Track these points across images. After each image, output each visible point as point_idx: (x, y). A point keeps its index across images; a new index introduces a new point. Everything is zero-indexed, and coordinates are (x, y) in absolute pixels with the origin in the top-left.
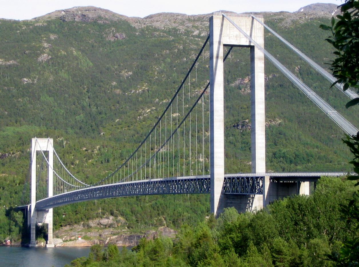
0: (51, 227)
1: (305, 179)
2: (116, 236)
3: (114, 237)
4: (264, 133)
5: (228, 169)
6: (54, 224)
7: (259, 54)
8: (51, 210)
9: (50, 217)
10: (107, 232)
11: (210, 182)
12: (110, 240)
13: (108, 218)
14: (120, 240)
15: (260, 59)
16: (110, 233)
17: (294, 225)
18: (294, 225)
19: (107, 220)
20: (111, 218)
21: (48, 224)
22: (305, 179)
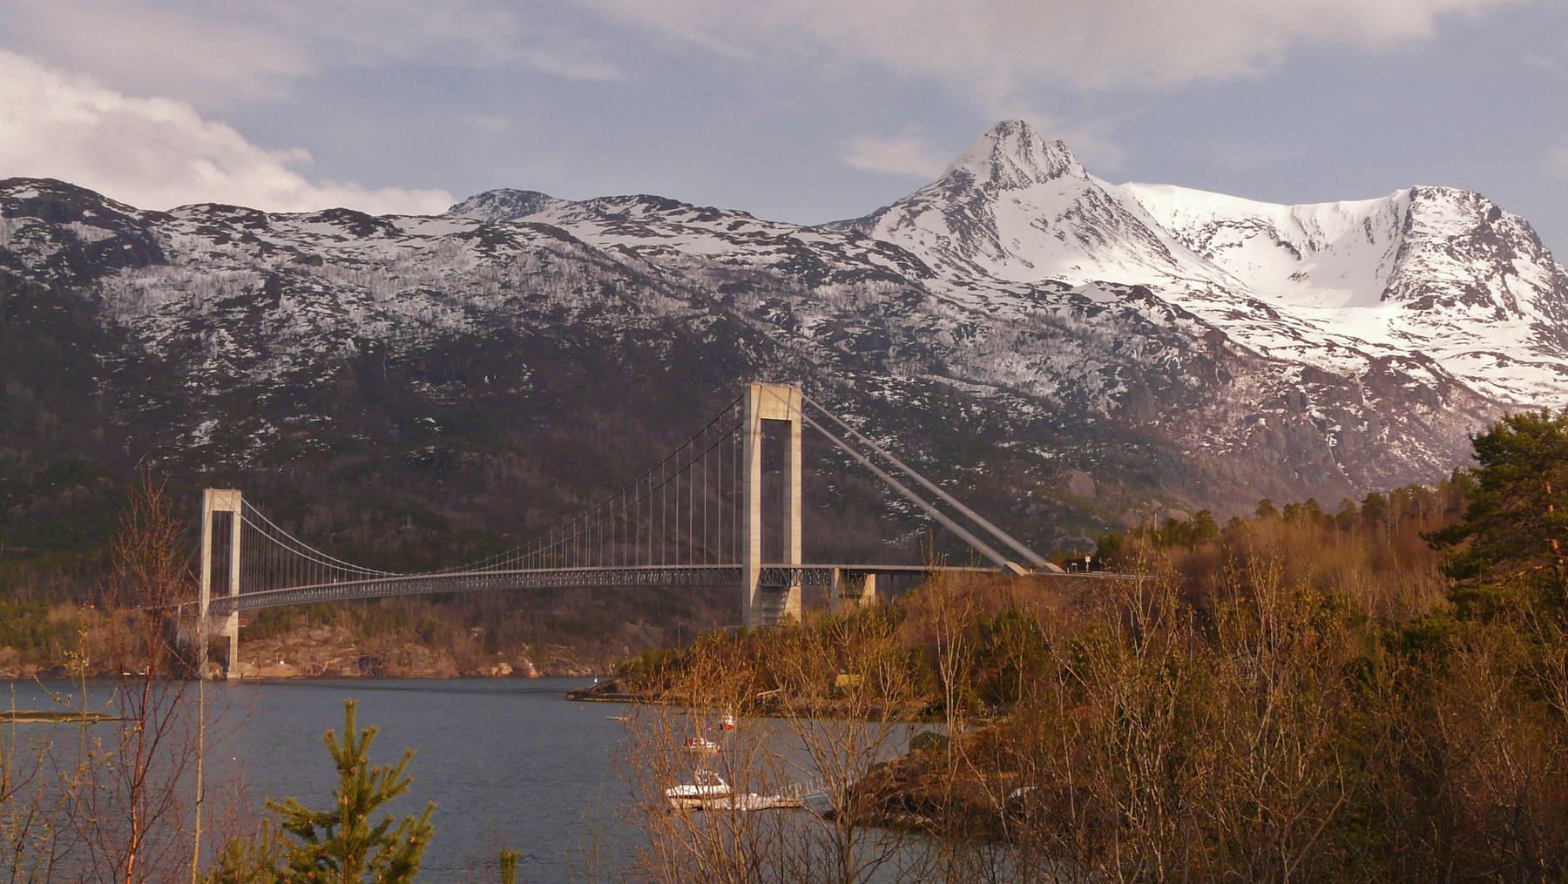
0: (234, 642)
1: (870, 571)
2: (340, 659)
3: (336, 660)
4: (800, 519)
5: (764, 559)
6: (241, 639)
7: (796, 429)
8: (236, 614)
9: (234, 625)
10: (322, 654)
11: (741, 574)
12: (330, 665)
13: (319, 628)
14: (346, 666)
15: (797, 436)
16: (329, 653)
17: (1165, 320)
18: (1165, 320)
19: (320, 632)
20: (327, 628)
21: (229, 638)
22: (870, 571)
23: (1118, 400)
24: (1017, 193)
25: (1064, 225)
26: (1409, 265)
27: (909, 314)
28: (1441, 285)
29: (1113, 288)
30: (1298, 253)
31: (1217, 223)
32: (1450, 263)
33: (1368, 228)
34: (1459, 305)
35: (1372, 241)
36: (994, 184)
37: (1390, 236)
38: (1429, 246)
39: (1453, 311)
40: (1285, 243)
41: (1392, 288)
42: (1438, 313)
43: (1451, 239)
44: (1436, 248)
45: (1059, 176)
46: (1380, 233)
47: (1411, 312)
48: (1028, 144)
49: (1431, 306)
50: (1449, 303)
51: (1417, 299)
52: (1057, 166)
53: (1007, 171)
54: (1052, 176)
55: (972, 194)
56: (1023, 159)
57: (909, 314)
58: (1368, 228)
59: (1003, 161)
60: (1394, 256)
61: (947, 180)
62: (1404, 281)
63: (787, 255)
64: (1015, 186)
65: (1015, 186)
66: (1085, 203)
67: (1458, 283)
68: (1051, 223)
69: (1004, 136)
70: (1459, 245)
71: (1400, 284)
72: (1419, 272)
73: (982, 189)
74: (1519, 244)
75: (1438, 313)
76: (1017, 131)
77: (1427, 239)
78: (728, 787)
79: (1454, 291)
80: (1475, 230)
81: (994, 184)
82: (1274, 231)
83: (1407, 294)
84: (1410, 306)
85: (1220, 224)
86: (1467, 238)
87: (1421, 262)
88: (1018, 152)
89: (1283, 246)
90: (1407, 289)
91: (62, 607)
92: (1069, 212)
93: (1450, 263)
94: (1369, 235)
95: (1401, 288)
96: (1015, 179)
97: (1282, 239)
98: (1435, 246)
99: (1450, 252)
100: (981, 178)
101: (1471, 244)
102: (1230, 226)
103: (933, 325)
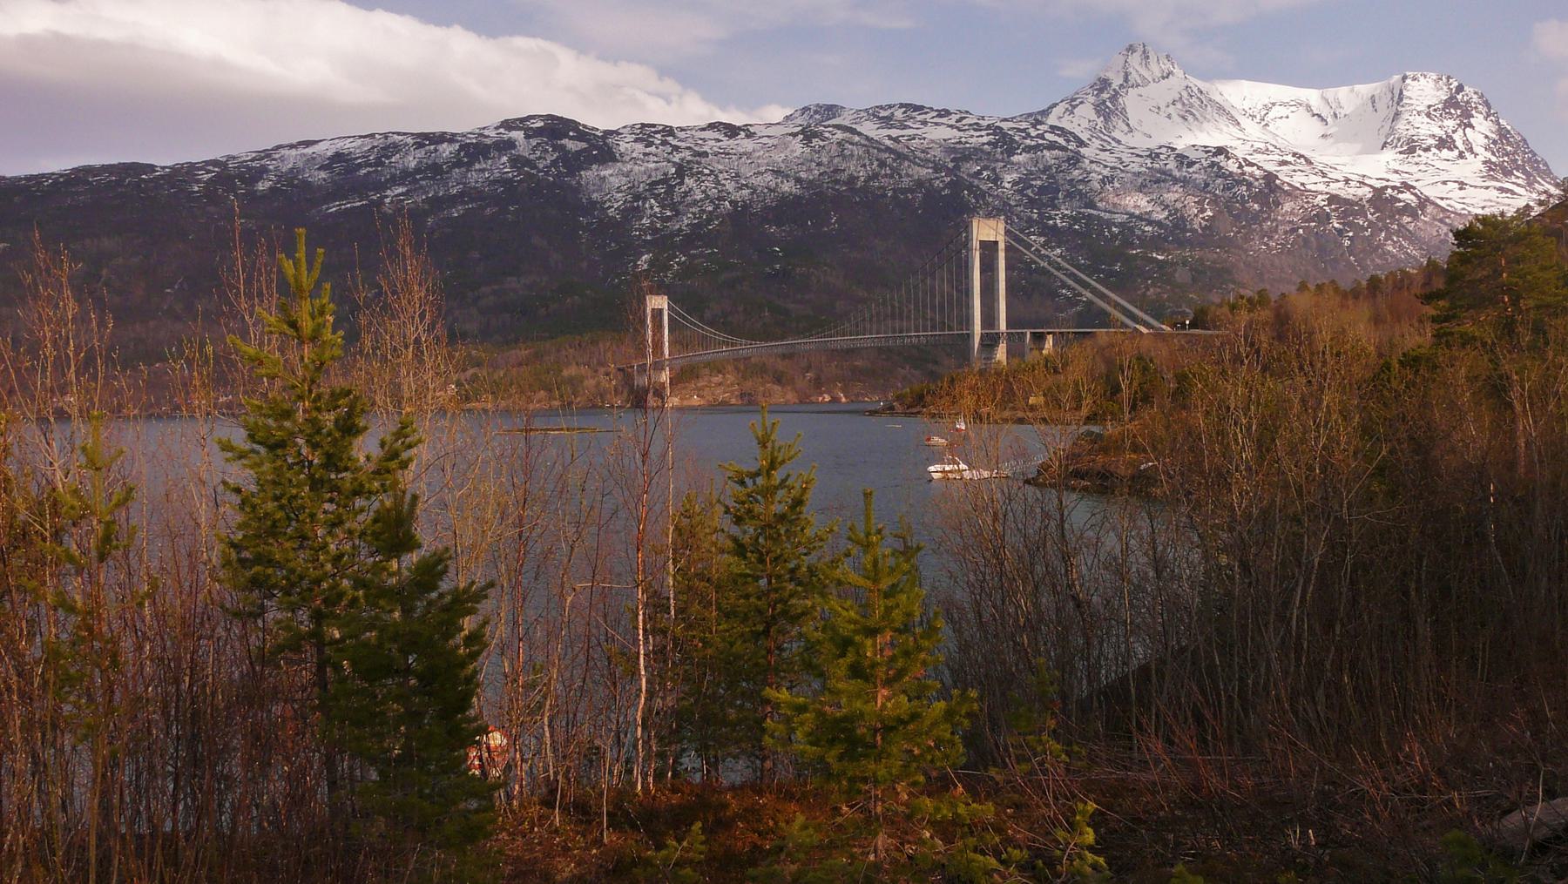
23: (1207, 220)
25: (1171, 109)
33: (1374, 102)
34: (1434, 150)
39: (1429, 154)
47: (1402, 156)
48: (1148, 57)
50: (1427, 149)
51: (1405, 148)
53: (1134, 77)
58: (1374, 102)
66: (1185, 94)
68: (1163, 108)
75: (1419, 156)
79: (1431, 141)
84: (1401, 153)
87: (1409, 123)
95: (1395, 141)
96: (1139, 82)
97: (1315, 112)
99: (1428, 115)
100: (1117, 81)
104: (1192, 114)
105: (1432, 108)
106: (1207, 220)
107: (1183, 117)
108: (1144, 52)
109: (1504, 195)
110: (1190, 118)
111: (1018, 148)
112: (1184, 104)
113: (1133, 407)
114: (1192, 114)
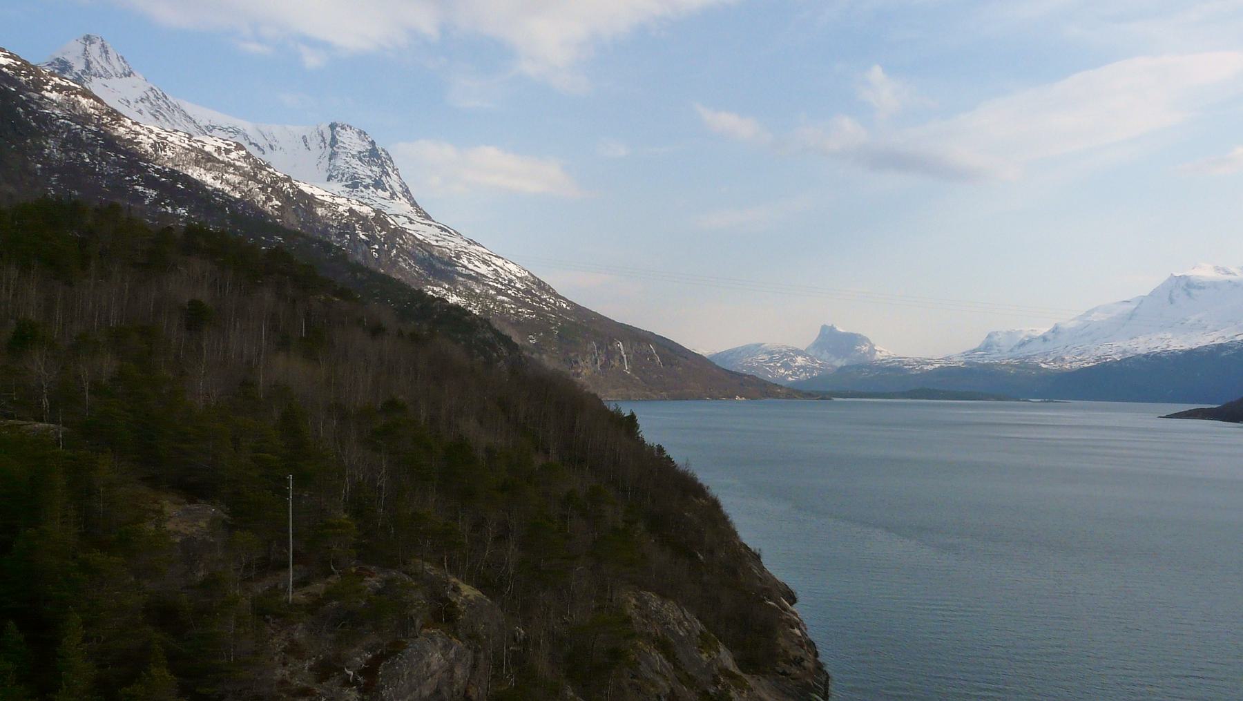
23: (276, 209)
24: (103, 80)
25: (140, 105)
26: (339, 162)
27: (115, 127)
28: (362, 177)
29: (222, 141)
30: (263, 150)
31: (213, 126)
32: (361, 166)
33: (305, 141)
34: (372, 189)
35: (309, 149)
36: (88, 71)
37: (321, 147)
38: (350, 155)
39: (370, 191)
40: (254, 144)
41: (334, 174)
42: (362, 192)
43: (360, 152)
44: (353, 156)
45: (129, 76)
46: (315, 143)
47: (348, 189)
48: (106, 52)
49: (358, 188)
50: (367, 187)
51: (350, 183)
52: (127, 69)
53: (95, 65)
54: (126, 76)
55: (74, 74)
56: (105, 61)
57: (115, 127)
58: (305, 141)
59: (91, 59)
60: (327, 158)
61: (53, 63)
62: (341, 171)
63: (14, 61)
64: (102, 76)
65: (102, 76)
66: (150, 94)
67: (370, 177)
68: (132, 103)
69: (90, 44)
70: (364, 156)
71: (338, 173)
72: (348, 168)
73: (80, 73)
74: (385, 162)
75: (362, 192)
76: (99, 43)
77: (348, 151)
78: (300, 624)
79: (368, 181)
80: (370, 150)
81: (88, 71)
82: (247, 136)
83: (344, 179)
84: (347, 186)
85: (214, 127)
86: (367, 154)
87: (347, 163)
88: (101, 56)
89: (253, 146)
90: (343, 176)
91: (770, 350)
92: (142, 99)
93: (361, 166)
94: (306, 145)
95: (340, 176)
96: (102, 72)
97: (252, 141)
98: (352, 155)
99: (360, 159)
100: (79, 66)
101: (369, 157)
102: (220, 129)
103: (136, 138)
104: (162, 114)
105: (362, 155)
106: (276, 209)
107: (154, 116)
108: (103, 46)
109: (443, 233)
110: (161, 118)
111: (47, 84)
112: (151, 103)
113: (578, 462)
114: (162, 114)
